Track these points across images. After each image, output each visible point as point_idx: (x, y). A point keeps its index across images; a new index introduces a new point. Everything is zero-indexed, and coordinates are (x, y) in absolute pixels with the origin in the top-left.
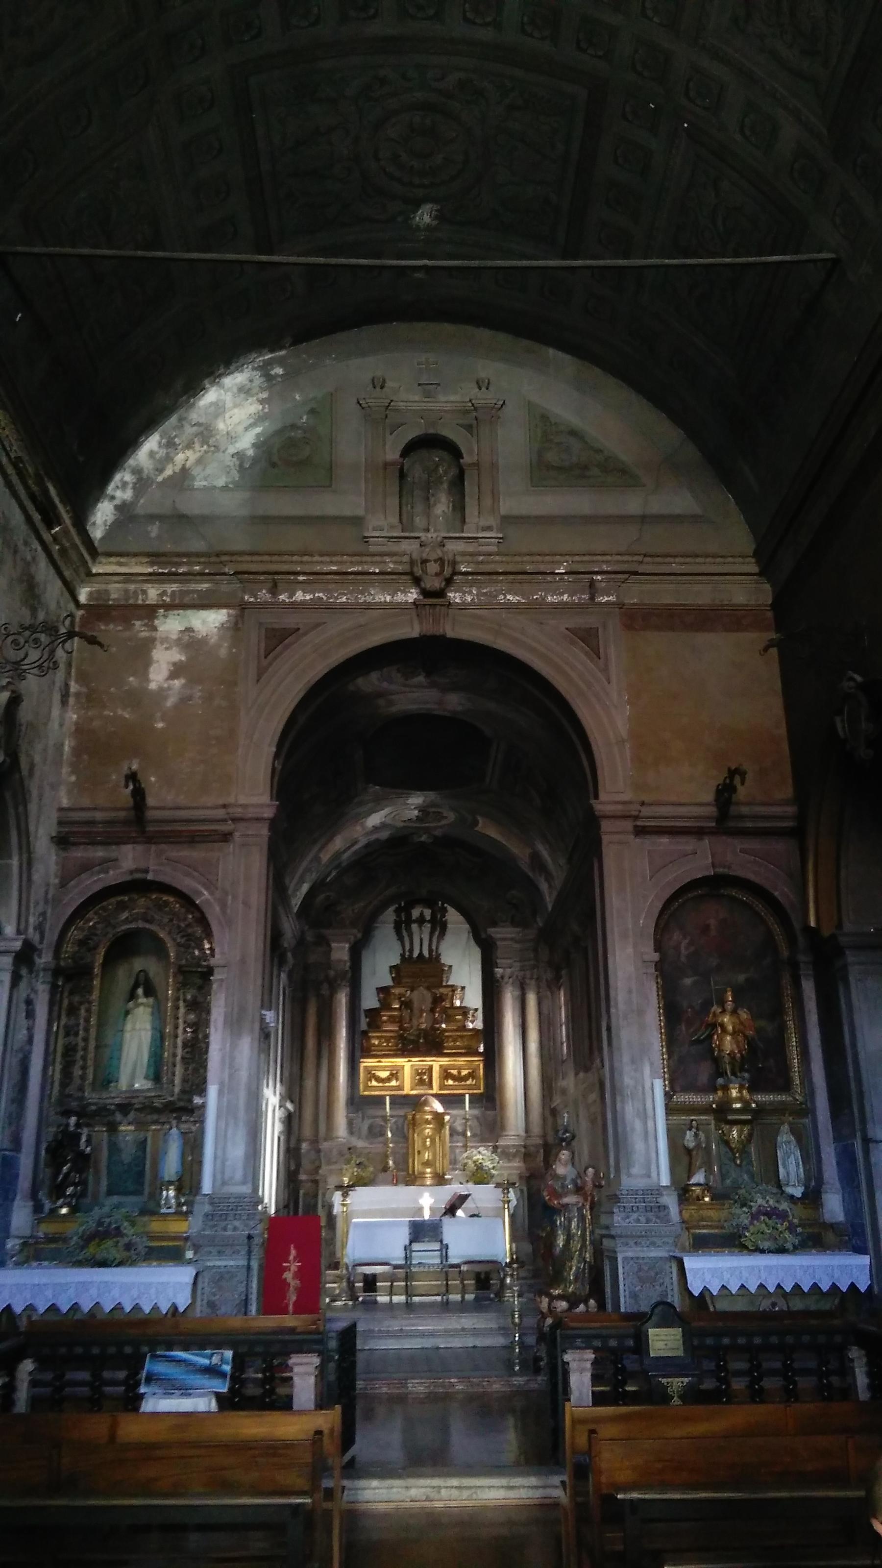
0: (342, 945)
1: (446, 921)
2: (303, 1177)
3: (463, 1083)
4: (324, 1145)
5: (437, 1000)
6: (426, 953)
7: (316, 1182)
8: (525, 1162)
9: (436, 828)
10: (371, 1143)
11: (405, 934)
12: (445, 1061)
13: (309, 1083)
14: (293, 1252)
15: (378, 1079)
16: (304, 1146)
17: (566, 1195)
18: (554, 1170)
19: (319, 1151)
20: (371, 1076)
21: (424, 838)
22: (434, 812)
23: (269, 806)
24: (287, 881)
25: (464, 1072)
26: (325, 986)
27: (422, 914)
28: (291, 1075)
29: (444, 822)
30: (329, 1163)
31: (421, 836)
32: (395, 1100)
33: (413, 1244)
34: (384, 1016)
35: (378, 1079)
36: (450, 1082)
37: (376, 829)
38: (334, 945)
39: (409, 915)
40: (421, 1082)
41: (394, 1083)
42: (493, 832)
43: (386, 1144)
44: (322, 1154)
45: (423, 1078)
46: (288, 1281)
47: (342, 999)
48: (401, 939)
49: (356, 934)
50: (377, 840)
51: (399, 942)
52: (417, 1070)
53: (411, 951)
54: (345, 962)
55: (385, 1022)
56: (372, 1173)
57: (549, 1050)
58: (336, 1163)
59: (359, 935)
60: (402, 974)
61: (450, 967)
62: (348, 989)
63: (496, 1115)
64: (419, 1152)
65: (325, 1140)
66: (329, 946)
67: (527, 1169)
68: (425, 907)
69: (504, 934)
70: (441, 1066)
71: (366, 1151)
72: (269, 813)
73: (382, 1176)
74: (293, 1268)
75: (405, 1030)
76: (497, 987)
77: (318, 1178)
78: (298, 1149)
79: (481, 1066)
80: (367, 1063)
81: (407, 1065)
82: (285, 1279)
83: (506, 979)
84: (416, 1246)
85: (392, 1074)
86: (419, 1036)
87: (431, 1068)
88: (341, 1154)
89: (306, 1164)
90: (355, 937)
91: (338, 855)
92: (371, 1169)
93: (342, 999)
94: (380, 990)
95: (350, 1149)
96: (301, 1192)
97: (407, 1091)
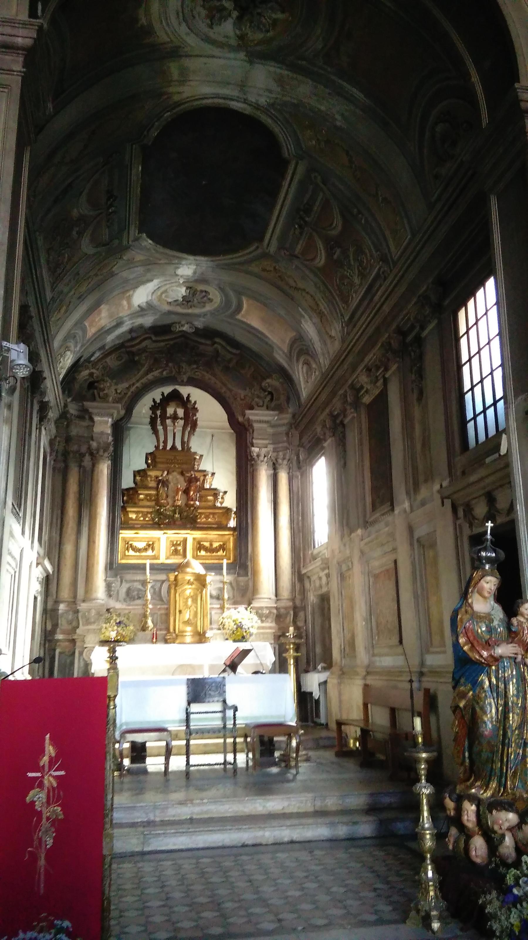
0: (106, 419)
1: (196, 420)
2: (59, 636)
3: (215, 554)
4: (83, 607)
5: (191, 481)
6: (179, 447)
7: (73, 641)
8: (276, 623)
9: (198, 316)
10: (129, 605)
11: (160, 428)
12: (198, 534)
13: (69, 548)
14: (50, 750)
15: (135, 549)
16: (62, 607)
17: (497, 644)
18: (471, 606)
19: (77, 612)
20: (129, 546)
21: (186, 328)
22: (202, 291)
23: (24, 25)
24: (53, 330)
25: (216, 545)
26: (87, 458)
27: (175, 412)
28: (50, 539)
29: (208, 308)
30: (88, 622)
31: (183, 326)
32: (153, 567)
33: (192, 705)
34: (141, 494)
35: (135, 549)
36: (203, 553)
37: (142, 311)
38: (96, 419)
39: (164, 412)
40: (176, 552)
41: (150, 553)
42: (255, 322)
43: (145, 605)
44: (80, 615)
45: (178, 549)
46: (38, 808)
47: (104, 469)
48: (155, 431)
49: (119, 411)
50: (141, 327)
51: (154, 436)
52: (172, 541)
53: (165, 442)
54: (108, 434)
55: (143, 500)
56: (132, 631)
57: (298, 524)
58: (94, 623)
59: (123, 412)
60: (158, 460)
61: (201, 456)
62: (110, 462)
63: (248, 581)
64: (180, 612)
65: (84, 601)
66: (92, 419)
67: (279, 629)
68: (178, 406)
69: (260, 417)
70: (194, 539)
71: (127, 612)
72: (24, 38)
73: (141, 634)
74: (49, 781)
75: (161, 506)
76: (252, 465)
77: (75, 637)
78: (55, 610)
79: (232, 538)
80: (125, 534)
81: (164, 538)
82: (33, 803)
83: (262, 458)
84: (195, 707)
85: (149, 545)
86: (174, 512)
87: (185, 541)
88: (99, 614)
89: (63, 624)
90: (118, 412)
91: (104, 332)
92: (132, 628)
93: (104, 469)
94: (137, 473)
95: (108, 610)
96: (57, 652)
97: (162, 560)
